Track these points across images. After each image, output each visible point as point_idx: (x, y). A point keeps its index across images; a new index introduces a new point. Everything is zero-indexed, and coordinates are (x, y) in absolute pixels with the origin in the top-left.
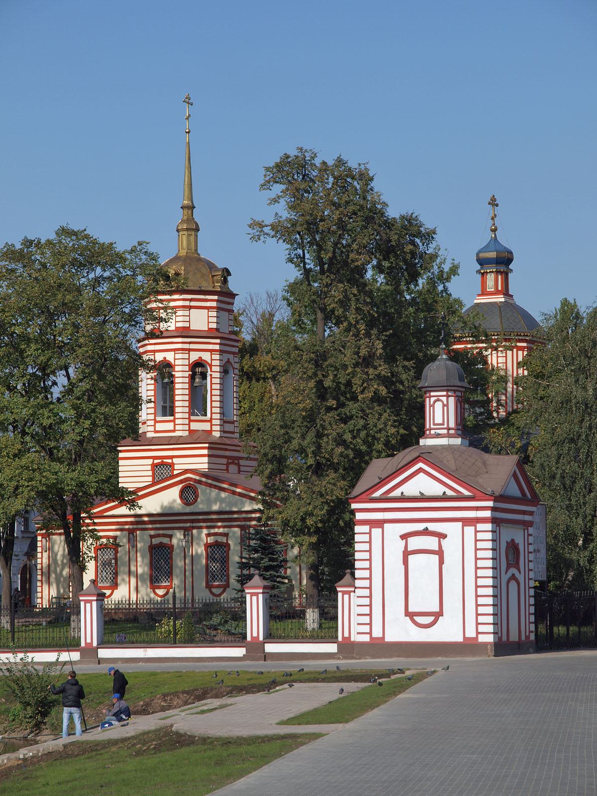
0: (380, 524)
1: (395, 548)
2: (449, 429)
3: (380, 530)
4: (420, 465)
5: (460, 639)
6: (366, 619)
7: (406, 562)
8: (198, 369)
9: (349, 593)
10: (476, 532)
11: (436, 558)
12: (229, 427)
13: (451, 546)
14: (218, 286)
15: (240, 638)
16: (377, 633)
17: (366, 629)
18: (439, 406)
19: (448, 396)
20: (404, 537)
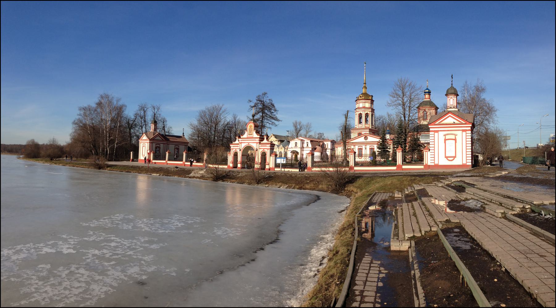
0: (437, 131)
1: (442, 138)
6: (433, 159)
7: (445, 142)
8: (367, 115)
13: (459, 138)
15: (395, 165)
16: (436, 163)
17: (433, 161)
20: (445, 135)
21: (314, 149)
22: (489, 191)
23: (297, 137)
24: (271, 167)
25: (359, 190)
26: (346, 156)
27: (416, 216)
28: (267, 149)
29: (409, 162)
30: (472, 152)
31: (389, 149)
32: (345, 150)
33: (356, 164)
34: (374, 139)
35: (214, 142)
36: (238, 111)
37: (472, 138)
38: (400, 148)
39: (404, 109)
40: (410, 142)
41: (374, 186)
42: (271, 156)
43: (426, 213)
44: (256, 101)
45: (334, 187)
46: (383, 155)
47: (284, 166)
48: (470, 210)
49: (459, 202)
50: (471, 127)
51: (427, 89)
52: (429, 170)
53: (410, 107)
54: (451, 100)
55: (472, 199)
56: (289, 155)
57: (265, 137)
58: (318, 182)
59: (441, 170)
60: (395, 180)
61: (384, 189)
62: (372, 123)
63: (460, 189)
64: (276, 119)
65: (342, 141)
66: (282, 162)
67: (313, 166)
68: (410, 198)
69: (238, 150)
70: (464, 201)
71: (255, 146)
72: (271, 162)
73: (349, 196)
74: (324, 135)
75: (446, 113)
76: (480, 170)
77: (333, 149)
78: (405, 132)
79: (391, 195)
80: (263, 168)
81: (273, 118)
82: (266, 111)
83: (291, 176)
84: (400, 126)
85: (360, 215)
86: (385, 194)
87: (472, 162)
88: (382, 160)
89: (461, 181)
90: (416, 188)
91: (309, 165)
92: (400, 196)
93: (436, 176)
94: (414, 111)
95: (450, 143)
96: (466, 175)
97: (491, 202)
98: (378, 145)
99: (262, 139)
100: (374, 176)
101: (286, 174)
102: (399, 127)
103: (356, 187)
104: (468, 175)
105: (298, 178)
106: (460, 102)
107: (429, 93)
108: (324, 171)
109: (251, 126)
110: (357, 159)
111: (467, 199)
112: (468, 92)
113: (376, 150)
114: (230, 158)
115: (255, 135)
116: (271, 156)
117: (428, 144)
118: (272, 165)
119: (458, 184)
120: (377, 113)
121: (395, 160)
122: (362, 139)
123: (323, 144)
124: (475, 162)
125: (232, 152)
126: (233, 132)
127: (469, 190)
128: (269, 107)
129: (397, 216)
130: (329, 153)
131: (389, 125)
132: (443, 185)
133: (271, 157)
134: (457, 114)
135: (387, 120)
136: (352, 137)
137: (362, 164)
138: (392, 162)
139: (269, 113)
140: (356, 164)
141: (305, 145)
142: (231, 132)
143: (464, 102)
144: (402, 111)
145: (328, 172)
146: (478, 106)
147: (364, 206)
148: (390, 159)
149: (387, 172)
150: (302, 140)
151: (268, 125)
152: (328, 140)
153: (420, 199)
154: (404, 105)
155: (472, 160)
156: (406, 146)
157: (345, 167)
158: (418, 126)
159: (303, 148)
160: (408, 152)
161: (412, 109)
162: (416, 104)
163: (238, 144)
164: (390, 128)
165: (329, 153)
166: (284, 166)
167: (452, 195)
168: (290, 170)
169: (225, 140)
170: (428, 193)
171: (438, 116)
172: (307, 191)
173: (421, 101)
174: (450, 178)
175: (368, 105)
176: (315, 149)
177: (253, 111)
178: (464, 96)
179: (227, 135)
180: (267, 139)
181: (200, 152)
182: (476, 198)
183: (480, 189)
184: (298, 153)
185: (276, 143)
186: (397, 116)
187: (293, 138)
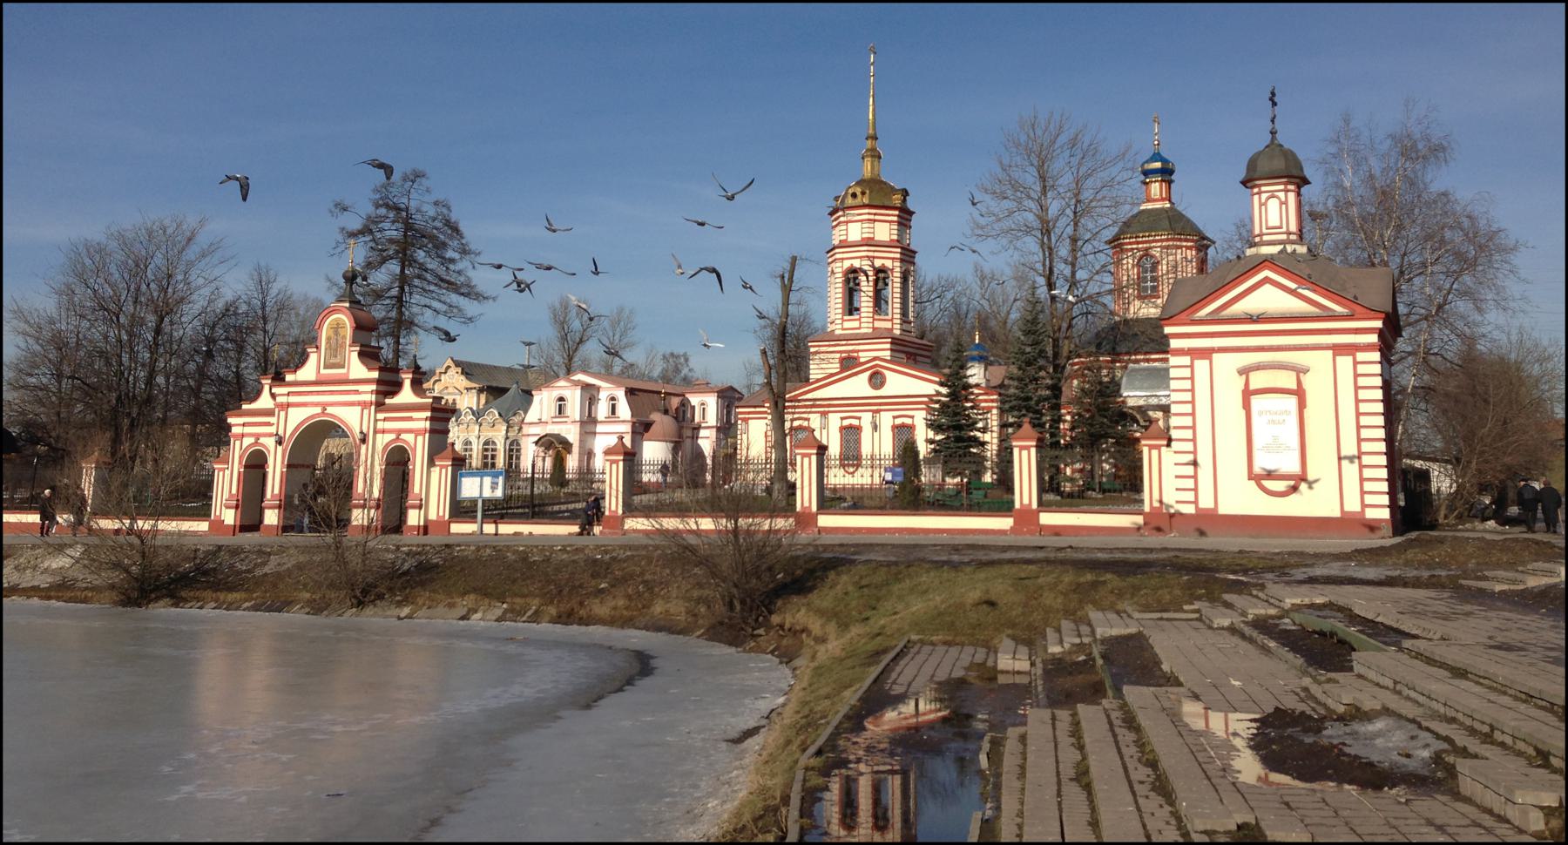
0: (1206, 353)
1: (1230, 389)
2: (1289, 233)
3: (1207, 362)
4: (1266, 273)
5: (1337, 513)
6: (1190, 483)
8: (881, 274)
9: (1158, 447)
10: (1356, 363)
11: (1292, 401)
12: (905, 326)
14: (898, 203)
15: (1005, 508)
16: (1206, 502)
17: (1190, 496)
18: (1273, 205)
19: (1287, 191)
20: (1245, 372)
21: (642, 428)
22: (1479, 679)
23: (569, 372)
24: (433, 516)
25: (832, 628)
26: (783, 466)
27: (1088, 788)
28: (417, 432)
29: (1071, 495)
30: (1392, 454)
31: (984, 430)
32: (780, 435)
33: (831, 500)
34: (925, 386)
35: (149, 400)
36: (289, 253)
37: (1386, 386)
38: (1027, 427)
39: (1049, 251)
40: (1077, 401)
41: (908, 608)
42: (431, 463)
43: (1141, 773)
44: (370, 209)
45: (720, 608)
46: (953, 461)
47: (495, 511)
48: (1373, 777)
49: (1316, 726)
50: (1381, 333)
51: (1157, 157)
52: (1172, 539)
53: (1074, 240)
54: (1273, 205)
55: (1386, 711)
56: (530, 455)
57: (407, 379)
58: (650, 589)
59: (1229, 543)
60: (999, 586)
61: (951, 627)
62: (904, 313)
63: (1324, 650)
64: (470, 292)
65: (766, 394)
66: (487, 493)
67: (630, 509)
68: (1067, 682)
69: (270, 442)
70: (1341, 719)
71: (352, 418)
72: (431, 490)
73: (787, 657)
74: (691, 364)
75: (1244, 269)
76: (1438, 553)
77: (727, 429)
78: (1056, 355)
79: (980, 655)
80: (394, 523)
81: (452, 287)
82: (420, 255)
83: (524, 558)
84: (1031, 326)
85: (814, 762)
86: (954, 651)
87: (1393, 506)
88: (952, 481)
89: (1330, 606)
90: (1099, 632)
91: (613, 503)
92: (1024, 665)
93: (1204, 567)
94: (1095, 256)
95: (1274, 413)
96: (1362, 573)
97: (1488, 738)
98: (929, 410)
99: (387, 386)
100: (909, 558)
101: (499, 551)
102: (1027, 333)
103: (821, 612)
104: (1371, 573)
105: (557, 570)
106: (1320, 208)
107: (1166, 173)
108: (676, 533)
109: (337, 327)
110: (837, 478)
111: (1356, 714)
112: (1357, 165)
113: (923, 438)
114: (226, 482)
115: (357, 369)
116: (431, 463)
117: (1166, 409)
118: (437, 508)
119: (1314, 622)
120: (929, 268)
121: (1005, 481)
122: (858, 386)
123: (685, 404)
124: (1412, 505)
125: (237, 452)
126: (254, 349)
127: (1370, 660)
128: (432, 238)
129: (998, 775)
130: (707, 442)
131: (983, 323)
132: (1237, 620)
133: (435, 471)
134: (1300, 269)
135: (976, 300)
136: (815, 374)
137: (857, 502)
138: (997, 493)
139: (432, 264)
140: (831, 500)
141: (602, 410)
142: (240, 349)
143: (1343, 206)
144: (1037, 257)
145: (692, 540)
146: (1413, 231)
147: (843, 710)
148: (988, 478)
149: (970, 539)
150: (586, 387)
151: (427, 318)
152: (705, 388)
153: (1119, 694)
154: (1047, 232)
155: (1392, 493)
156: (1059, 419)
157: (773, 512)
158: (1114, 327)
159: (594, 421)
160: (1068, 446)
161: (1088, 248)
162: (1103, 224)
163: (269, 413)
164: (990, 337)
165: (707, 442)
166: (495, 511)
167: (1284, 680)
168: (525, 529)
169: (209, 393)
170: (1158, 663)
171: (1209, 283)
172: (597, 632)
173: (1126, 212)
174: (1274, 589)
175: (885, 231)
176: (647, 426)
177: (356, 254)
178: (1339, 185)
179: (220, 368)
180: (417, 385)
181: (60, 456)
182: (1408, 710)
183: (1430, 661)
184: (567, 446)
185: (467, 401)
186: (1020, 279)
187: (548, 377)
